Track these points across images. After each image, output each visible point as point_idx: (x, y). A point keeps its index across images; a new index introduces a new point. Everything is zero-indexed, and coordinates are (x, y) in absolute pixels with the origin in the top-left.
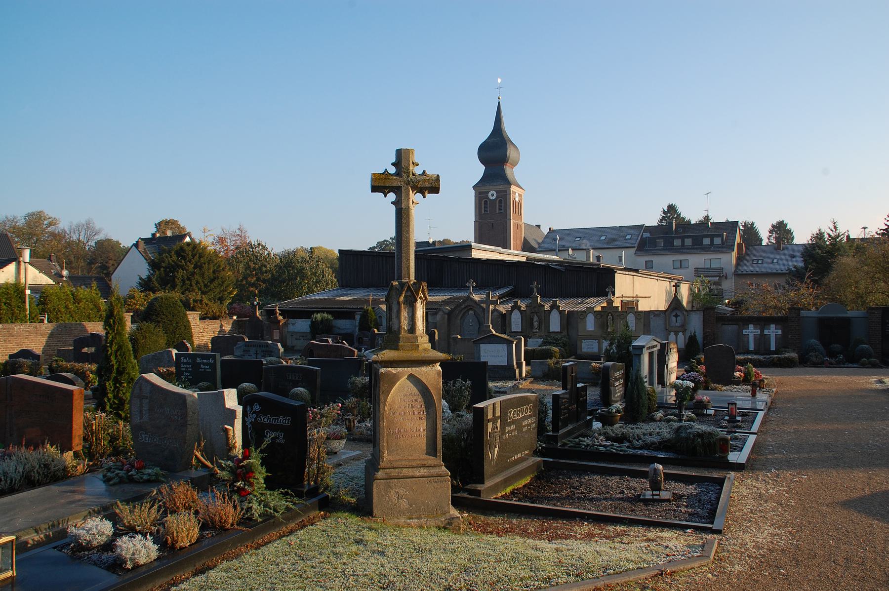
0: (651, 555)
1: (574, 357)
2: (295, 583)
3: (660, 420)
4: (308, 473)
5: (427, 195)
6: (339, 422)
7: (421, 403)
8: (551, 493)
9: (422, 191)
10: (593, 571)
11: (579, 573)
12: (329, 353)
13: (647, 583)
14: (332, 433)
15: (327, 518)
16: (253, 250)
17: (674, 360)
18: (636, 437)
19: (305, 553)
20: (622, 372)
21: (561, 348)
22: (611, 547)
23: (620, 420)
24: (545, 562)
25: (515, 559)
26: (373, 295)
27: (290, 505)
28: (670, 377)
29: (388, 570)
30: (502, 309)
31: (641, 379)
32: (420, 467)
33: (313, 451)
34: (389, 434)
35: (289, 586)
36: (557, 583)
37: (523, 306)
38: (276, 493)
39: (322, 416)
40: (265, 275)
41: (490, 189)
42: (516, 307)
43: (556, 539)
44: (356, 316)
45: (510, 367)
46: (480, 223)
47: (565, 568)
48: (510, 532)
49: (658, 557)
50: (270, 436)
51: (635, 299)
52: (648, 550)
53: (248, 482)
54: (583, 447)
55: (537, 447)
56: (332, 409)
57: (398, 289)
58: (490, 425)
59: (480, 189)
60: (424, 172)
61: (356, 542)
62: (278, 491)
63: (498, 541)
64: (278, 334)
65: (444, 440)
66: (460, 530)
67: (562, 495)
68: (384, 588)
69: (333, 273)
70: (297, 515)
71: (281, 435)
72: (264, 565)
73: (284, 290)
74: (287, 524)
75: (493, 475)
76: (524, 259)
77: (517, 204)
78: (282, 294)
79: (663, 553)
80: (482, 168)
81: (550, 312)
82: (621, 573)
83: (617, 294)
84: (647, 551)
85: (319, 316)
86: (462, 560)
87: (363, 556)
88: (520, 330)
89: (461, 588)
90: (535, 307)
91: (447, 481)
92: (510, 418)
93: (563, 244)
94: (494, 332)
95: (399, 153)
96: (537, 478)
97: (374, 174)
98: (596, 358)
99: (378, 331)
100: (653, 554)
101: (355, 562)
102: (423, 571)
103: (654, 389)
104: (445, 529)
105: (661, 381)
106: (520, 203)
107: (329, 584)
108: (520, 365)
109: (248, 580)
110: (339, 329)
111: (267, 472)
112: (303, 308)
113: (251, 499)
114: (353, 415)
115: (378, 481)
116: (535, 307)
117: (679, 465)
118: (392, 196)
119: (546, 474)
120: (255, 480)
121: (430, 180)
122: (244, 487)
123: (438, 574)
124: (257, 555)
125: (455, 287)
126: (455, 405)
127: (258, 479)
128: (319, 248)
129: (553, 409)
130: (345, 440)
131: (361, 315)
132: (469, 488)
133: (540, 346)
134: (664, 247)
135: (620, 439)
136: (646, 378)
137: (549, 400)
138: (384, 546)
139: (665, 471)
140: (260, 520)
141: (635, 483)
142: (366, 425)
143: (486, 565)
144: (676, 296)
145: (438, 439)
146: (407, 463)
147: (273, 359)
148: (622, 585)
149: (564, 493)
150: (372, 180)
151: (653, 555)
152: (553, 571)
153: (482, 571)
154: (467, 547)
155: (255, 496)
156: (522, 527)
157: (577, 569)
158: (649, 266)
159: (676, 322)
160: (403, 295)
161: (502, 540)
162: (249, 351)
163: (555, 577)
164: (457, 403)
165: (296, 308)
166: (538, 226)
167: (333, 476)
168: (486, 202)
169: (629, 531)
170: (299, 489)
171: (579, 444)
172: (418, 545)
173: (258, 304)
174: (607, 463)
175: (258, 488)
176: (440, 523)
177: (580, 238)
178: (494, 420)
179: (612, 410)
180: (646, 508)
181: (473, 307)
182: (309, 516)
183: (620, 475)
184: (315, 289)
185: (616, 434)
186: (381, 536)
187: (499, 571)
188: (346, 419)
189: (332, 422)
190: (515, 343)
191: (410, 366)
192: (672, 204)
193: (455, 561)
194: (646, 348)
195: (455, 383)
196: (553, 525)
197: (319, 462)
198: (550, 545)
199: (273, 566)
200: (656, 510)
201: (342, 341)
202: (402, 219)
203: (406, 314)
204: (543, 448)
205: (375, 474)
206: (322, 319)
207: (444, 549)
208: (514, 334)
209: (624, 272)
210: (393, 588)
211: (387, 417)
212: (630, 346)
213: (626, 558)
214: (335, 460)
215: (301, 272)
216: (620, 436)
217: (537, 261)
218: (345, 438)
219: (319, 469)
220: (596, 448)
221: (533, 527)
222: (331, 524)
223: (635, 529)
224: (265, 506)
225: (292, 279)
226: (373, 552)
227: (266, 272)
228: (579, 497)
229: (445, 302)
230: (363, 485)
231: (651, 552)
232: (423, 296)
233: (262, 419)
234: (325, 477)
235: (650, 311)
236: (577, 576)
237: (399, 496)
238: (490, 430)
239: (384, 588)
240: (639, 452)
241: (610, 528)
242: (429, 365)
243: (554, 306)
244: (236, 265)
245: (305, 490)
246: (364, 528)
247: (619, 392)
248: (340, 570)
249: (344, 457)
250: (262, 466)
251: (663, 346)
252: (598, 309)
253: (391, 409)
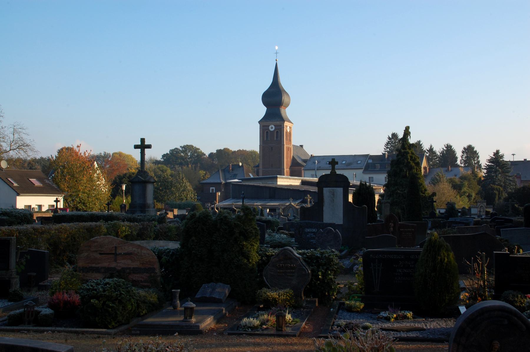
41: (270, 124)
59: (264, 123)
77: (288, 134)
106: (290, 133)
134: (380, 169)
166: (302, 146)
168: (267, 132)
192: (395, 133)
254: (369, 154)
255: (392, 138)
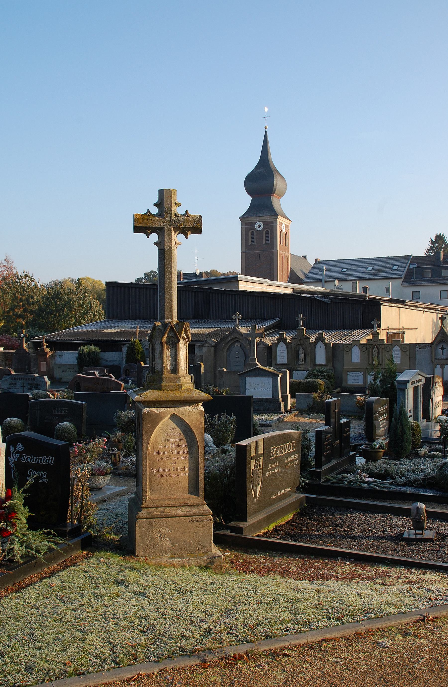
0: (412, 599)
1: (339, 389)
2: (55, 628)
3: (425, 456)
4: (71, 511)
5: (190, 236)
6: (105, 457)
7: (184, 443)
8: (314, 530)
9: (184, 231)
10: (353, 614)
11: (339, 617)
12: (95, 386)
13: (408, 629)
14: (97, 469)
15: (89, 557)
16: (19, 281)
17: (440, 394)
18: (400, 473)
19: (66, 596)
20: (386, 407)
21: (327, 381)
22: (372, 589)
23: (384, 455)
24: (305, 604)
25: (276, 600)
26: (140, 327)
27: (53, 545)
28: (435, 411)
29: (148, 612)
30: (268, 341)
31: (405, 414)
32: (183, 506)
33: (77, 489)
34: (151, 474)
35: (49, 631)
36: (317, 627)
37: (288, 337)
38: (38, 533)
39: (88, 451)
40: (32, 306)
42: (281, 339)
43: (318, 579)
44: (123, 349)
45: (275, 400)
46: (246, 255)
47: (326, 611)
48: (272, 571)
49: (420, 601)
50: (33, 476)
51: (401, 331)
52: (409, 593)
53: (11, 522)
54: (346, 483)
55: (300, 483)
56: (97, 444)
57: (161, 330)
58: (253, 463)
60: (186, 212)
61: (117, 583)
62: (41, 531)
63: (259, 581)
64: (45, 366)
65: (206, 477)
66: (221, 569)
67: (324, 532)
68: (144, 632)
69: (100, 304)
70: (59, 555)
71: (44, 475)
72: (24, 609)
73: (51, 321)
74: (49, 565)
75: (257, 511)
76: (290, 291)
77: (284, 235)
78: (50, 326)
79: (425, 596)
80: (249, 199)
81: (315, 344)
82: (382, 617)
83: (383, 326)
84: (409, 595)
85: (86, 349)
86: (222, 602)
87: (124, 597)
88: (285, 362)
89: (221, 631)
90: (300, 340)
91: (209, 520)
92: (273, 455)
93: (330, 275)
94: (259, 366)
95: (161, 193)
96: (300, 514)
97: (136, 215)
98: (361, 390)
99: (145, 363)
100: (415, 597)
101: (116, 604)
102: (184, 613)
103: (418, 424)
104: (206, 568)
105: (427, 415)
106: (286, 235)
107: (88, 628)
108: (285, 398)
109: (6, 626)
110: (107, 361)
111: (29, 512)
112: (70, 340)
113: (13, 540)
114: (118, 450)
115: (141, 520)
116: (300, 340)
117: (443, 504)
118: (154, 237)
119: (309, 511)
120: (17, 521)
121: (192, 221)
122: (7, 527)
123: (198, 617)
124: (17, 598)
125: (221, 319)
126: (220, 439)
127: (20, 519)
128: (87, 279)
129: (316, 444)
130: (111, 475)
131: (128, 347)
132: (231, 525)
133: (306, 378)
134: (431, 277)
135: (383, 476)
136: (410, 412)
137: (312, 436)
138: (145, 587)
139: (428, 509)
140: (21, 561)
141: (398, 521)
142: (131, 460)
143: (246, 607)
144: (442, 329)
145: (200, 479)
146: (170, 502)
147: (40, 392)
148: (383, 630)
149: (326, 531)
150: (135, 220)
151: (415, 599)
152: (314, 613)
153: (242, 613)
154: (228, 588)
155: (17, 537)
156: (284, 566)
157: (338, 612)
158: (416, 297)
159: (443, 354)
160: (166, 336)
161: (264, 580)
162: (15, 384)
163: (315, 620)
164: (221, 437)
165: (63, 340)
166: (305, 257)
167: (98, 512)
168: (253, 233)
169: (391, 572)
170: (61, 529)
171: (342, 480)
172: (180, 585)
173: (25, 336)
174: (370, 500)
175: (20, 529)
176: (202, 563)
177: (347, 269)
178: (257, 458)
179: (375, 446)
180: (409, 548)
181: (239, 339)
182: (71, 556)
183: (383, 513)
184: (83, 321)
185: (379, 471)
186: (143, 576)
187: (259, 614)
188: (112, 454)
189: (98, 456)
190: (280, 376)
191: (172, 406)
192: (440, 234)
193: (215, 603)
194: (410, 383)
195: (219, 417)
196: (315, 564)
197: (82, 500)
198: (311, 586)
199: (32, 610)
200: (419, 550)
201: (109, 374)
202: (164, 260)
203: (169, 355)
204: (306, 484)
205: (138, 513)
206: (89, 352)
207: (205, 590)
208: (280, 366)
209: (390, 304)
210: (154, 631)
211: (149, 457)
212: (395, 380)
213: (387, 601)
214: (99, 496)
215: (68, 304)
216: (383, 472)
217: (303, 293)
218: (110, 474)
219: (82, 507)
220: (359, 484)
221: (294, 566)
222: (93, 564)
223: (397, 570)
224: (27, 547)
225: (60, 310)
226: (135, 593)
227: (33, 303)
228: (341, 535)
229: (211, 335)
230: (127, 522)
231: (413, 595)
232: (185, 337)
233: (26, 458)
234: (88, 516)
235: (416, 343)
236: (338, 619)
237: (161, 535)
238: (252, 467)
239: (144, 632)
240: (402, 489)
241: (372, 568)
242: (192, 405)
243: (320, 339)
244: (3, 296)
245: (69, 529)
246: (126, 568)
247: (383, 427)
248: (100, 613)
249: (108, 493)
250: (24, 506)
251: (428, 380)
252: (364, 341)
253: (153, 449)
254: (411, 255)
255: (437, 241)
